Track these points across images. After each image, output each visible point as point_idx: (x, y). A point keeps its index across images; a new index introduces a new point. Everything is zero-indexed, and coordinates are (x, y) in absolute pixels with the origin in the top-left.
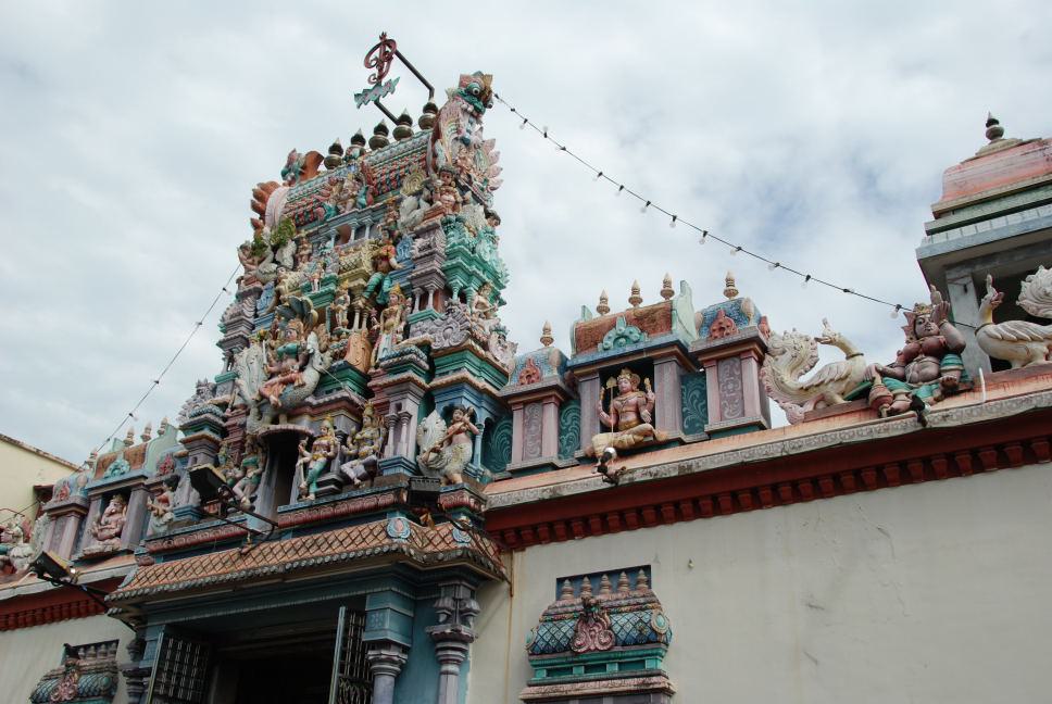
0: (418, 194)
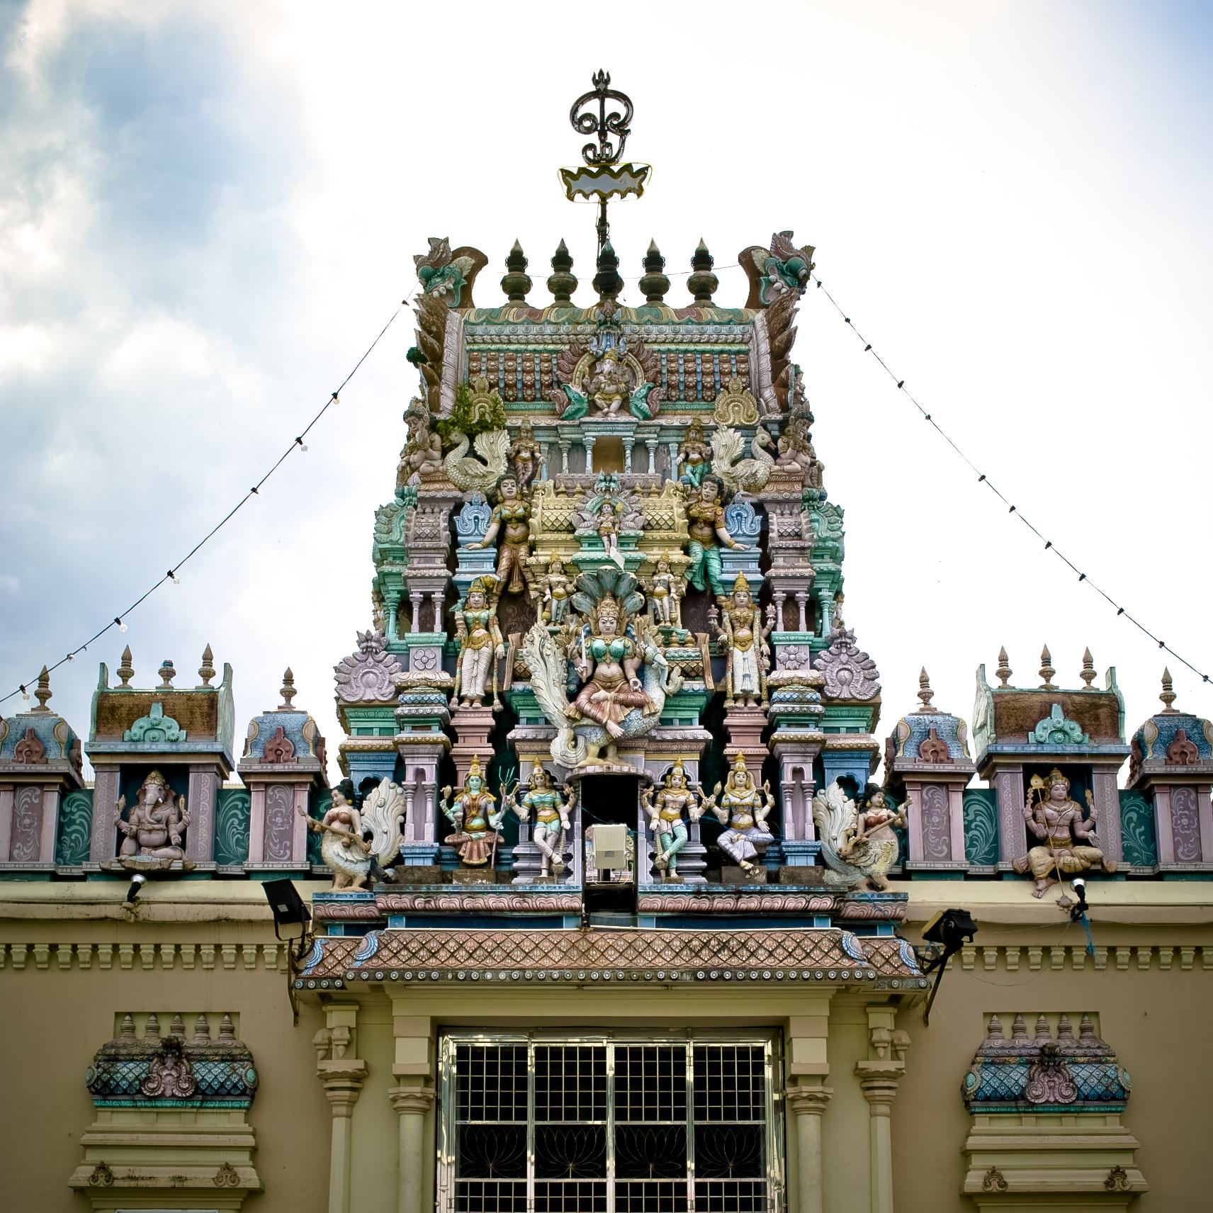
0: (748, 430)
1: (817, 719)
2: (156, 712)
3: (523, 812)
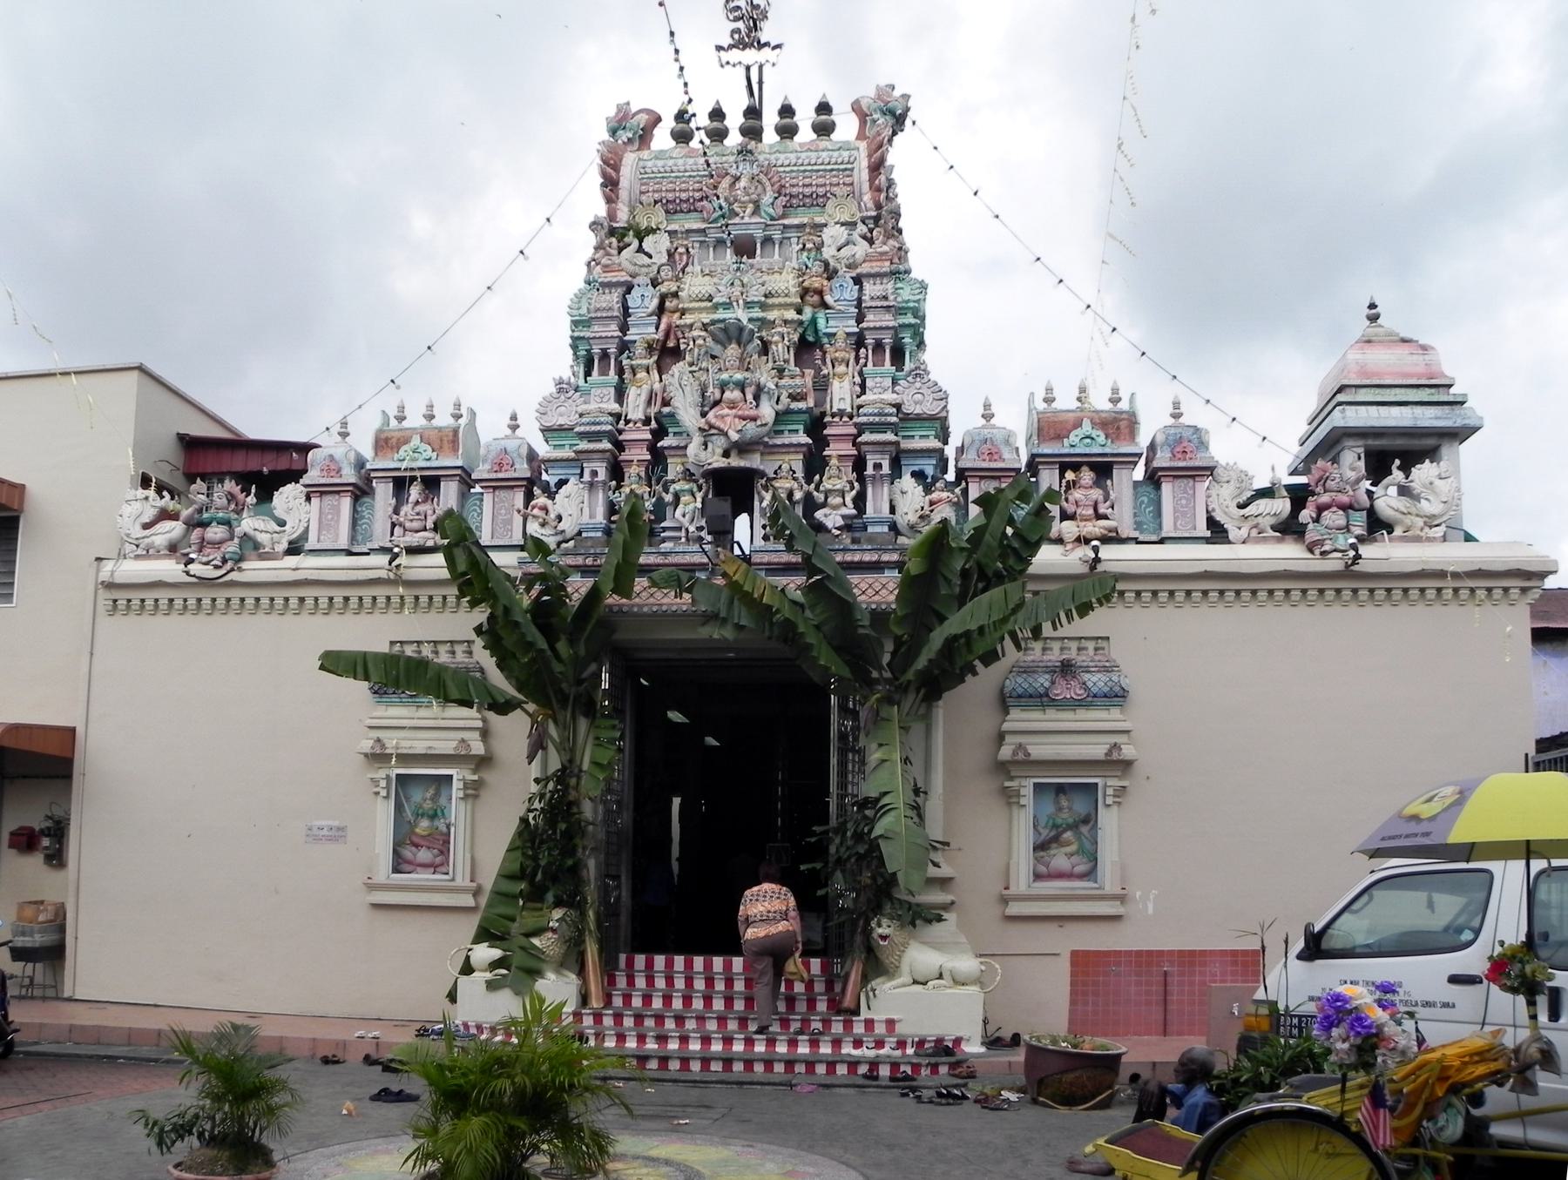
1: (893, 427)
2: (416, 441)
3: (668, 498)
